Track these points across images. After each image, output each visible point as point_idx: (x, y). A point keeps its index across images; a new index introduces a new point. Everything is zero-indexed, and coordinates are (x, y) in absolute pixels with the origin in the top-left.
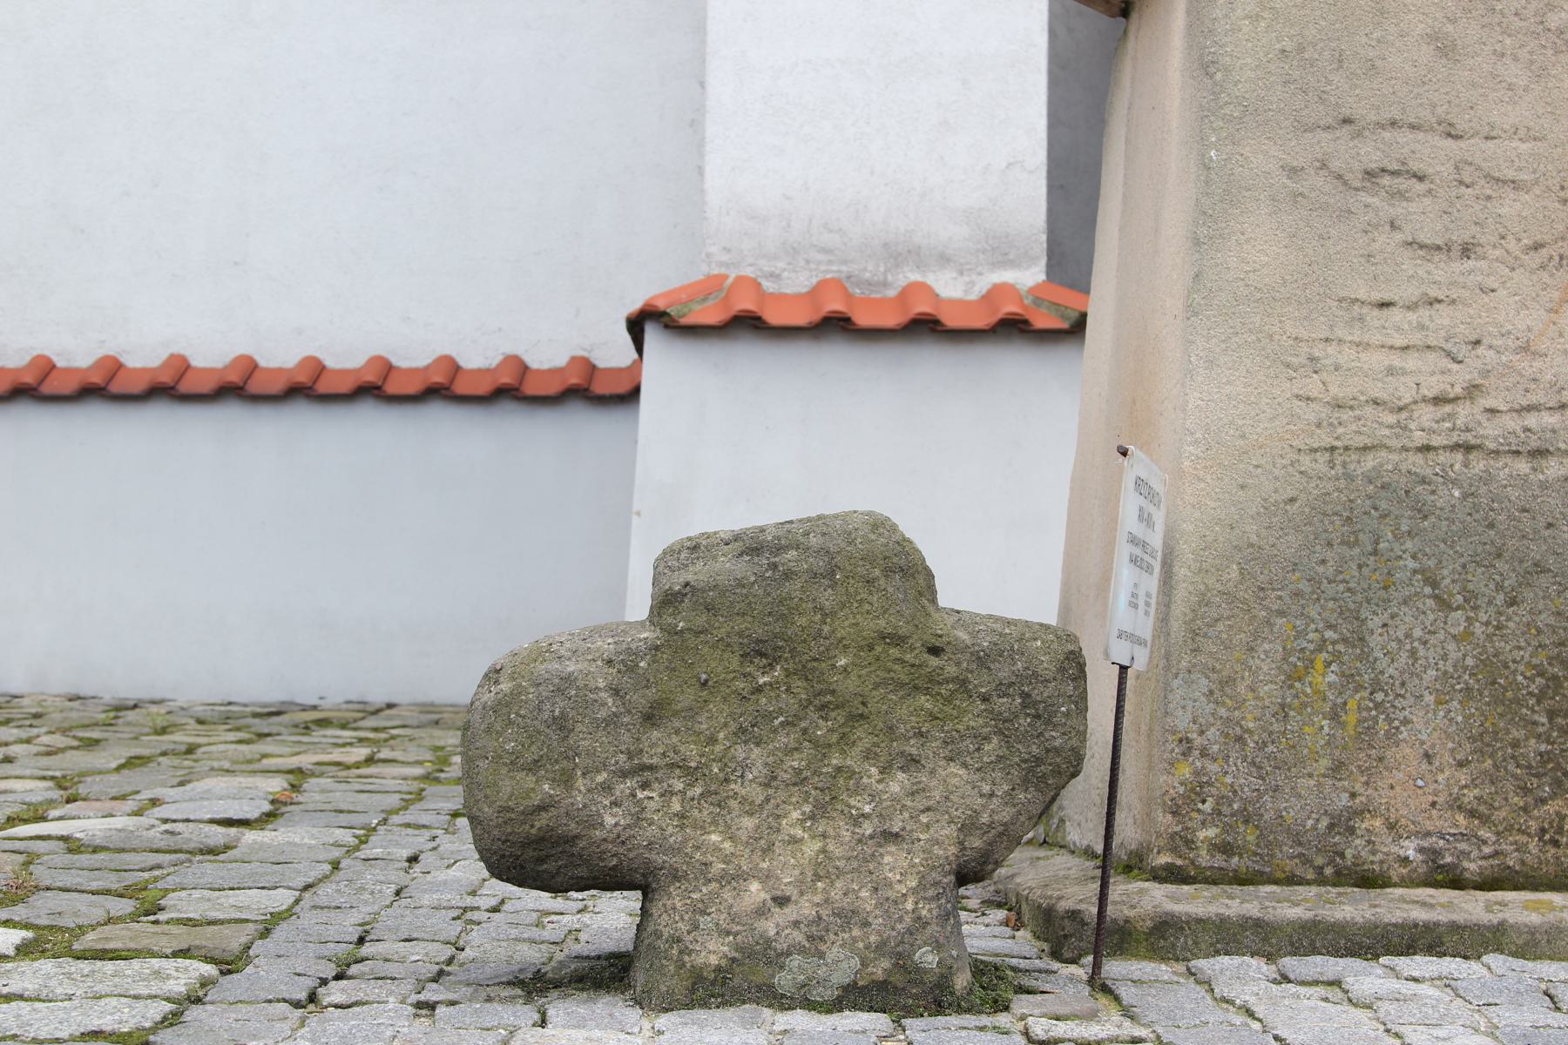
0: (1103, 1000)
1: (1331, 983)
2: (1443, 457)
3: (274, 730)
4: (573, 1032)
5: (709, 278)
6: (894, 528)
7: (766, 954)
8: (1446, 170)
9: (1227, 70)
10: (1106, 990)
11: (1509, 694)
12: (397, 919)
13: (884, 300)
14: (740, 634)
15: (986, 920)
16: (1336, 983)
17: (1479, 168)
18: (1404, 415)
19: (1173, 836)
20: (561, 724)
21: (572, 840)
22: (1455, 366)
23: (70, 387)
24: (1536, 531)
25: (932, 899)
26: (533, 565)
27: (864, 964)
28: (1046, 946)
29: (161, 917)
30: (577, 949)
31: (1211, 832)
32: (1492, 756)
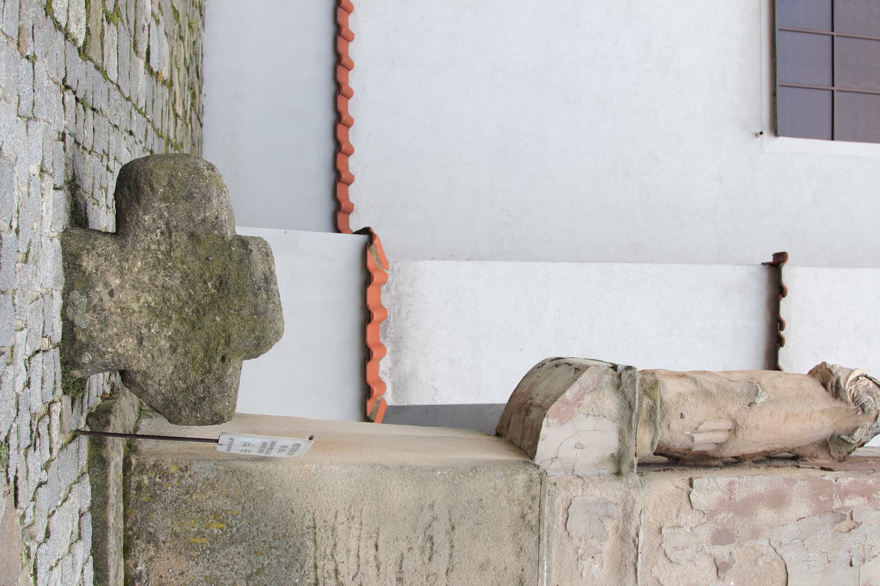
0: (69, 436)
1: (80, 535)
2: (312, 575)
3: (191, 74)
4: (51, 202)
5: (387, 263)
6: (277, 341)
8: (433, 569)
10: (74, 437)
12: (104, 125)
13: (378, 337)
14: (229, 274)
15: (105, 384)
16: (80, 537)
18: (330, 557)
19: (144, 465)
20: (189, 197)
21: (138, 201)
25: (113, 359)
27: (83, 330)
28: (94, 411)
29: (105, 23)
31: (146, 481)
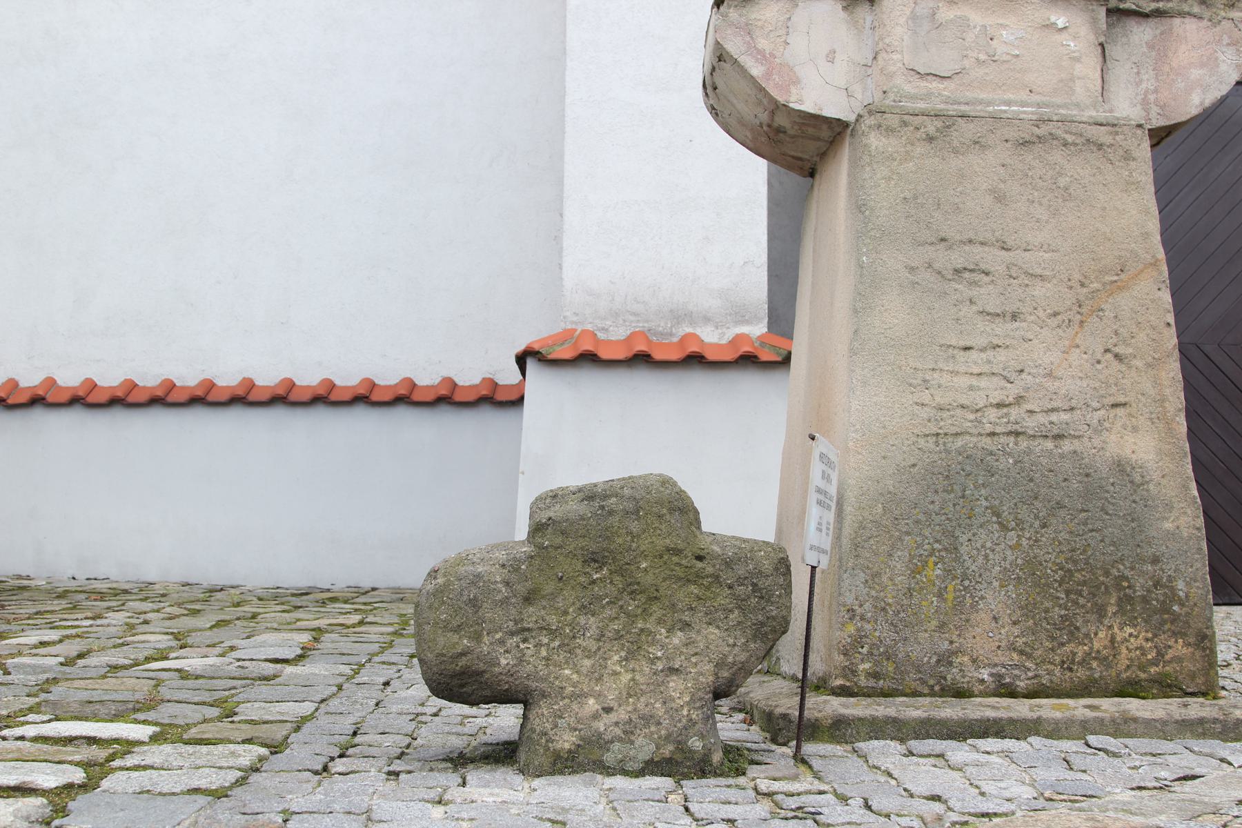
0: (802, 768)
1: (938, 756)
2: (1003, 439)
3: (304, 604)
5: (565, 331)
6: (675, 484)
7: (597, 742)
8: (1002, 269)
9: (872, 210)
10: (804, 761)
11: (1043, 581)
12: (376, 720)
13: (670, 344)
14: (582, 548)
15: (732, 720)
16: (941, 756)
17: (1021, 268)
18: (979, 414)
19: (844, 668)
20: (474, 603)
22: (1009, 385)
23: (183, 398)
24: (1057, 483)
26: (447, 508)
28: (768, 735)
29: (236, 719)
30: (485, 739)
31: (867, 666)
32: (1033, 618)
